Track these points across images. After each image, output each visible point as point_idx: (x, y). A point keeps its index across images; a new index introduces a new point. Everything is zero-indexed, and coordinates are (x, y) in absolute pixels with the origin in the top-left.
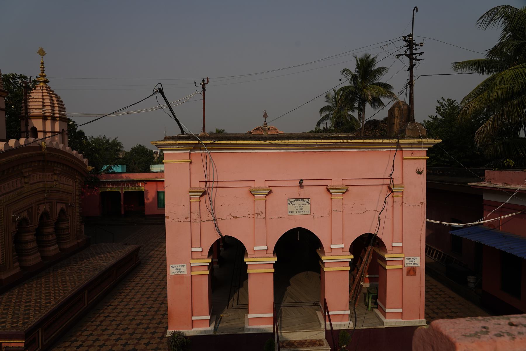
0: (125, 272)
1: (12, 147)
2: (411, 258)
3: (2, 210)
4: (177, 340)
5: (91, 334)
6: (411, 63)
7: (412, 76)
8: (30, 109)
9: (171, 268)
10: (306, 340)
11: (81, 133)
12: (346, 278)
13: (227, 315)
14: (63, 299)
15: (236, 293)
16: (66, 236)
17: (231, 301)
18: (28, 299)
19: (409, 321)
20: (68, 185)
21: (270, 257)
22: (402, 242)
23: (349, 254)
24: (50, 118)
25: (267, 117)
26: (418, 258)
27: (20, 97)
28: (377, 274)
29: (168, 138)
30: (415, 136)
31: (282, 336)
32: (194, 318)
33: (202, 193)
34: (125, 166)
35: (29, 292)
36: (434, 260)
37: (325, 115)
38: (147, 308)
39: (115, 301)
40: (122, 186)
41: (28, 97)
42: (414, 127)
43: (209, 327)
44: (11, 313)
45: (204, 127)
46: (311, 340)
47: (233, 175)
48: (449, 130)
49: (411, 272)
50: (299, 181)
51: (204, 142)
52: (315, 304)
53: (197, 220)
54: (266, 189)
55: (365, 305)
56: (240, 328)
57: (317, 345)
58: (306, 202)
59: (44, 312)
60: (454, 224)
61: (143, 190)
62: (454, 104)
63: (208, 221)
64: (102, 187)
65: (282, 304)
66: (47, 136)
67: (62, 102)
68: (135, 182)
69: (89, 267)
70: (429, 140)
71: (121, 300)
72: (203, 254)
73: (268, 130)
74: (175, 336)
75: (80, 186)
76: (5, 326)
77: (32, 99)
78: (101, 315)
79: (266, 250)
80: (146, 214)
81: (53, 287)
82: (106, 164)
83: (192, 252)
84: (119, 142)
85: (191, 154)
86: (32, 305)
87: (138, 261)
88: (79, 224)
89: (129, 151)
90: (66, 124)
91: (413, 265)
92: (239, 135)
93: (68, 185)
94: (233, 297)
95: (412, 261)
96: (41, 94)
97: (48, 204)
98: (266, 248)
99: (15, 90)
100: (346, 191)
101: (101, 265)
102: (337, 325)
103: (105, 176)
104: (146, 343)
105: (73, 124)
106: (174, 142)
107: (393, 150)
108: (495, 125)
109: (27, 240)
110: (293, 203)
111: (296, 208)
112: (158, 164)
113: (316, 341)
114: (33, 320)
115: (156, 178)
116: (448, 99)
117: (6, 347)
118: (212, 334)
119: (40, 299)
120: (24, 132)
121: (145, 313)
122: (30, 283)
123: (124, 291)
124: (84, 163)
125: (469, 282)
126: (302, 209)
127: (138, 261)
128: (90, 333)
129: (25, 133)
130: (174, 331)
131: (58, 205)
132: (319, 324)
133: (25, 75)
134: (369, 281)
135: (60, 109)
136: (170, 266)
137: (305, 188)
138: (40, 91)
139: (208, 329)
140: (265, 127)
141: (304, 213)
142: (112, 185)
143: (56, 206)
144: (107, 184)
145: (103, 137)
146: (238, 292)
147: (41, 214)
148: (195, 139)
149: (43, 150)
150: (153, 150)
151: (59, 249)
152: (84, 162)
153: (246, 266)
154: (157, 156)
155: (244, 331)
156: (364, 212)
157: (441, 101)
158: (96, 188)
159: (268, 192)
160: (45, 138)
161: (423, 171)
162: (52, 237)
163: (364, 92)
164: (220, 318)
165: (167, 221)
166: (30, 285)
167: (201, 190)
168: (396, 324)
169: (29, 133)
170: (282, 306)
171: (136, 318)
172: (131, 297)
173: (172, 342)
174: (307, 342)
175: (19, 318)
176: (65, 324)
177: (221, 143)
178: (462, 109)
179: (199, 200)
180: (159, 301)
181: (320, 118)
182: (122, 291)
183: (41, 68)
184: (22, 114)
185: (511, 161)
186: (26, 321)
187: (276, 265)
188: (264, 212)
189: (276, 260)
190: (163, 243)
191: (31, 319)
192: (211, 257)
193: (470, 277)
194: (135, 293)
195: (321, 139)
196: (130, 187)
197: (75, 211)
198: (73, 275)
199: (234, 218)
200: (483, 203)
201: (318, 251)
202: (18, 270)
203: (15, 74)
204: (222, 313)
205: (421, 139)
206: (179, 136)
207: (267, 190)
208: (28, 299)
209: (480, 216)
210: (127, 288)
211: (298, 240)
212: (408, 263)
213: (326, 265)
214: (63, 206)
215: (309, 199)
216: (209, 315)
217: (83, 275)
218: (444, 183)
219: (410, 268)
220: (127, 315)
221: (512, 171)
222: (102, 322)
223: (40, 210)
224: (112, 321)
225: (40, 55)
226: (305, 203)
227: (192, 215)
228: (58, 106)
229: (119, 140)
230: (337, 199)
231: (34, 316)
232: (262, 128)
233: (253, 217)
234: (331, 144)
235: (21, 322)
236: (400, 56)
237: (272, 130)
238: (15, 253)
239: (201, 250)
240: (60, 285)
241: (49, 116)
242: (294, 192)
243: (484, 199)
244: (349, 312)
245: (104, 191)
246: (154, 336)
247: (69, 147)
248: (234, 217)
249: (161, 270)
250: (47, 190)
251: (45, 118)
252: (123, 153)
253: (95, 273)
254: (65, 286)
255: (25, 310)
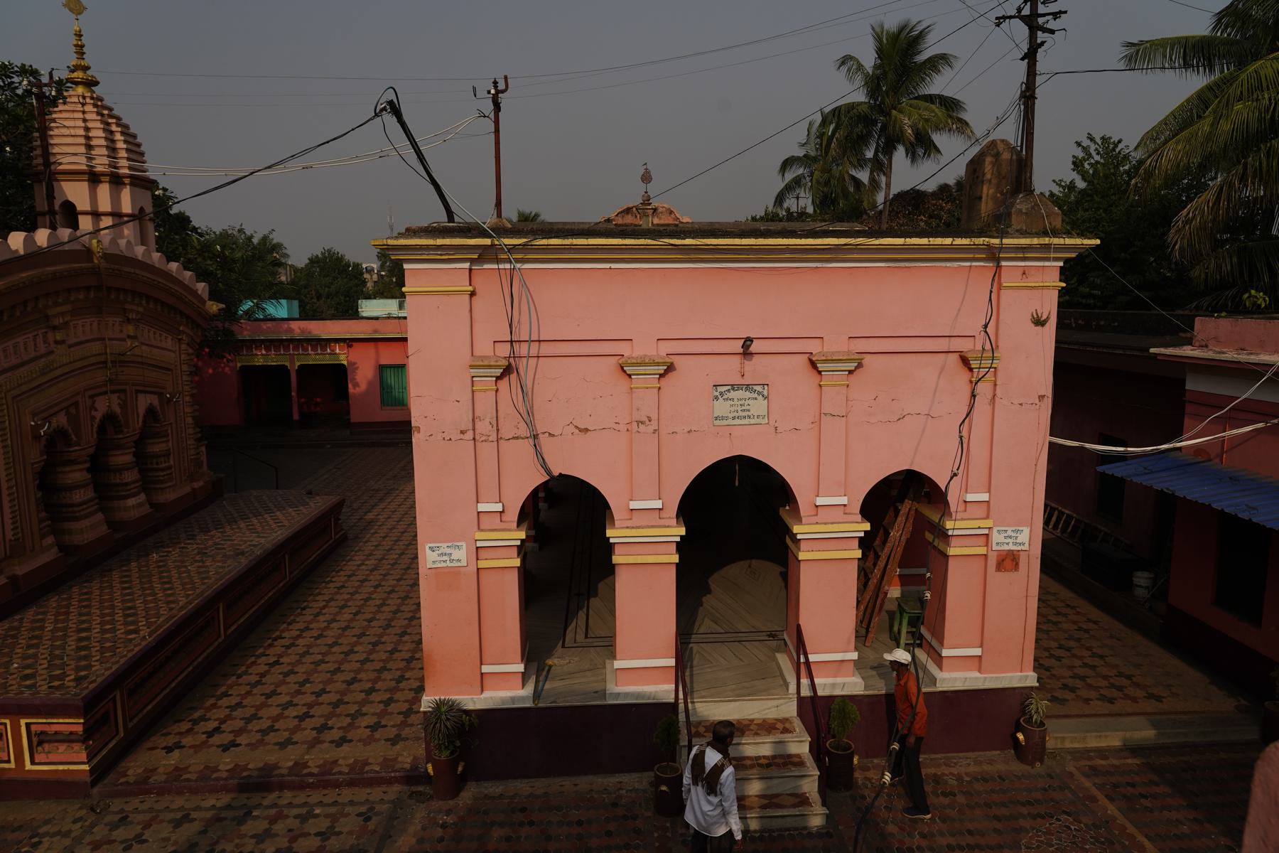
0: (311, 559)
1: (17, 251)
2: (1010, 529)
3: (3, 410)
4: (448, 719)
5: (239, 705)
6: (1033, 40)
7: (1032, 73)
8: (54, 154)
9: (428, 552)
10: (752, 721)
11: (183, 220)
12: (852, 572)
13: (562, 662)
14: (167, 623)
15: (582, 609)
16: (165, 473)
17: (570, 628)
18: (83, 622)
19: (997, 677)
20: (158, 348)
21: (668, 527)
22: (989, 491)
23: (860, 520)
24: (107, 179)
25: (650, 182)
26: (1026, 531)
27: (26, 124)
28: (923, 565)
29: (414, 229)
30: (1034, 231)
31: (696, 712)
32: (485, 669)
33: (502, 371)
34: (296, 303)
35: (85, 607)
36: (1053, 534)
37: (794, 179)
38: (369, 643)
39: (291, 627)
40: (291, 352)
41: (48, 123)
42: (1033, 208)
43: (523, 689)
44: (46, 655)
45: (498, 204)
46: (764, 720)
47: (578, 325)
48: (1104, 215)
49: (1008, 563)
50: (743, 340)
51: (507, 241)
52: (772, 635)
53: (489, 436)
54: (660, 361)
55: (891, 640)
56: (594, 692)
57: (755, 722)
58: (759, 393)
59: (125, 653)
60: (1114, 449)
61: (345, 363)
62: (1117, 150)
63: (517, 438)
64: (243, 355)
65: (693, 636)
66: (102, 225)
67: (134, 136)
68: (314, 343)
69: (224, 548)
70: (1069, 241)
71: (306, 625)
72: (505, 517)
73: (654, 213)
74: (443, 710)
75: (191, 351)
76: (34, 686)
77: (57, 127)
78: (259, 661)
79: (660, 509)
80: (352, 421)
81: (140, 596)
82: (250, 296)
83: (479, 513)
84: (278, 243)
85: (473, 271)
86: (94, 638)
87: (341, 533)
88: (193, 444)
89: (303, 266)
90: (149, 194)
91: (1011, 547)
92: (587, 226)
93: (158, 348)
94: (575, 620)
95: (1010, 537)
96: (80, 115)
97: (118, 394)
98: (658, 504)
99: (11, 105)
100: (857, 368)
101: (254, 543)
102: (825, 685)
103: (248, 328)
104: (372, 724)
105: (163, 194)
106: (429, 240)
107: (976, 266)
108: (1224, 204)
109: (70, 482)
110: (725, 397)
111: (732, 409)
112: (375, 298)
113: (774, 721)
114: (100, 672)
115: (376, 332)
116: (1103, 138)
117: (39, 734)
118: (529, 705)
119: (113, 622)
120: (43, 214)
121: (365, 656)
122: (85, 585)
123: (310, 605)
124: (198, 294)
125: (1137, 586)
126: (749, 411)
127: (341, 533)
128: (236, 702)
129: (47, 217)
130: (440, 699)
131: (141, 397)
132: (782, 683)
133: (33, 67)
134: (899, 583)
135: (131, 156)
136: (427, 547)
137: (756, 358)
138: (79, 107)
139: (518, 695)
140: (644, 207)
141: (752, 421)
142: (267, 349)
143: (137, 400)
144: (254, 346)
145: (237, 229)
146: (586, 608)
147: (100, 421)
148: (483, 233)
149: (96, 261)
150: (361, 265)
151: (150, 504)
152: (199, 292)
153: (609, 548)
154: (371, 279)
155: (605, 699)
156: (899, 419)
157: (1086, 143)
158: (227, 356)
159: (665, 367)
160: (97, 231)
161: (1047, 317)
162: (131, 476)
163: (893, 118)
164: (547, 668)
165: (416, 438)
166: (86, 590)
167: (499, 363)
168: (964, 683)
169: (57, 217)
170: (692, 640)
171: (343, 667)
172: (328, 617)
173: (436, 723)
174: (755, 724)
175: (66, 668)
176: (177, 681)
177: (547, 245)
178: (1141, 162)
179: (495, 387)
180: (397, 628)
181: (781, 186)
182: (305, 604)
183: (75, 46)
184: (36, 167)
185: (1261, 294)
186: (83, 673)
187: (682, 546)
188: (654, 417)
189: (684, 533)
190: (397, 492)
191: (93, 669)
192: (525, 525)
193: (1139, 574)
194: (337, 609)
195: (800, 234)
196: (310, 355)
197: (182, 414)
198: (186, 567)
199: (580, 431)
200: (1184, 399)
201: (784, 513)
202: (53, 554)
203: (7, 63)
204: (549, 655)
205: (1047, 237)
206: (443, 227)
207: (664, 364)
208: (83, 622)
209: (1177, 433)
210: (317, 598)
211: (737, 484)
212: (1002, 540)
213: (803, 545)
214: (154, 400)
215: (766, 387)
216: (522, 661)
217: (211, 565)
218: (1088, 349)
219: (1005, 553)
220: (323, 662)
221: (1261, 319)
222: (263, 675)
223: (96, 410)
224: (286, 674)
225: (71, 13)
226: (756, 395)
227: (479, 425)
228: (125, 146)
229: (276, 238)
230: (834, 386)
231: (101, 663)
232: (637, 209)
233: (628, 430)
234: (824, 249)
235: (72, 677)
236: (1004, 21)
237: (661, 213)
238: (43, 514)
239: (501, 510)
240: (156, 589)
241: (103, 174)
242: (729, 368)
243: (1187, 388)
244: (854, 656)
245: (305, 363)
246: (390, 709)
247: (160, 254)
248: (580, 430)
249: (396, 554)
250: (112, 362)
251: (94, 178)
252: (288, 269)
253: (240, 562)
254: (169, 592)
255: (79, 649)
